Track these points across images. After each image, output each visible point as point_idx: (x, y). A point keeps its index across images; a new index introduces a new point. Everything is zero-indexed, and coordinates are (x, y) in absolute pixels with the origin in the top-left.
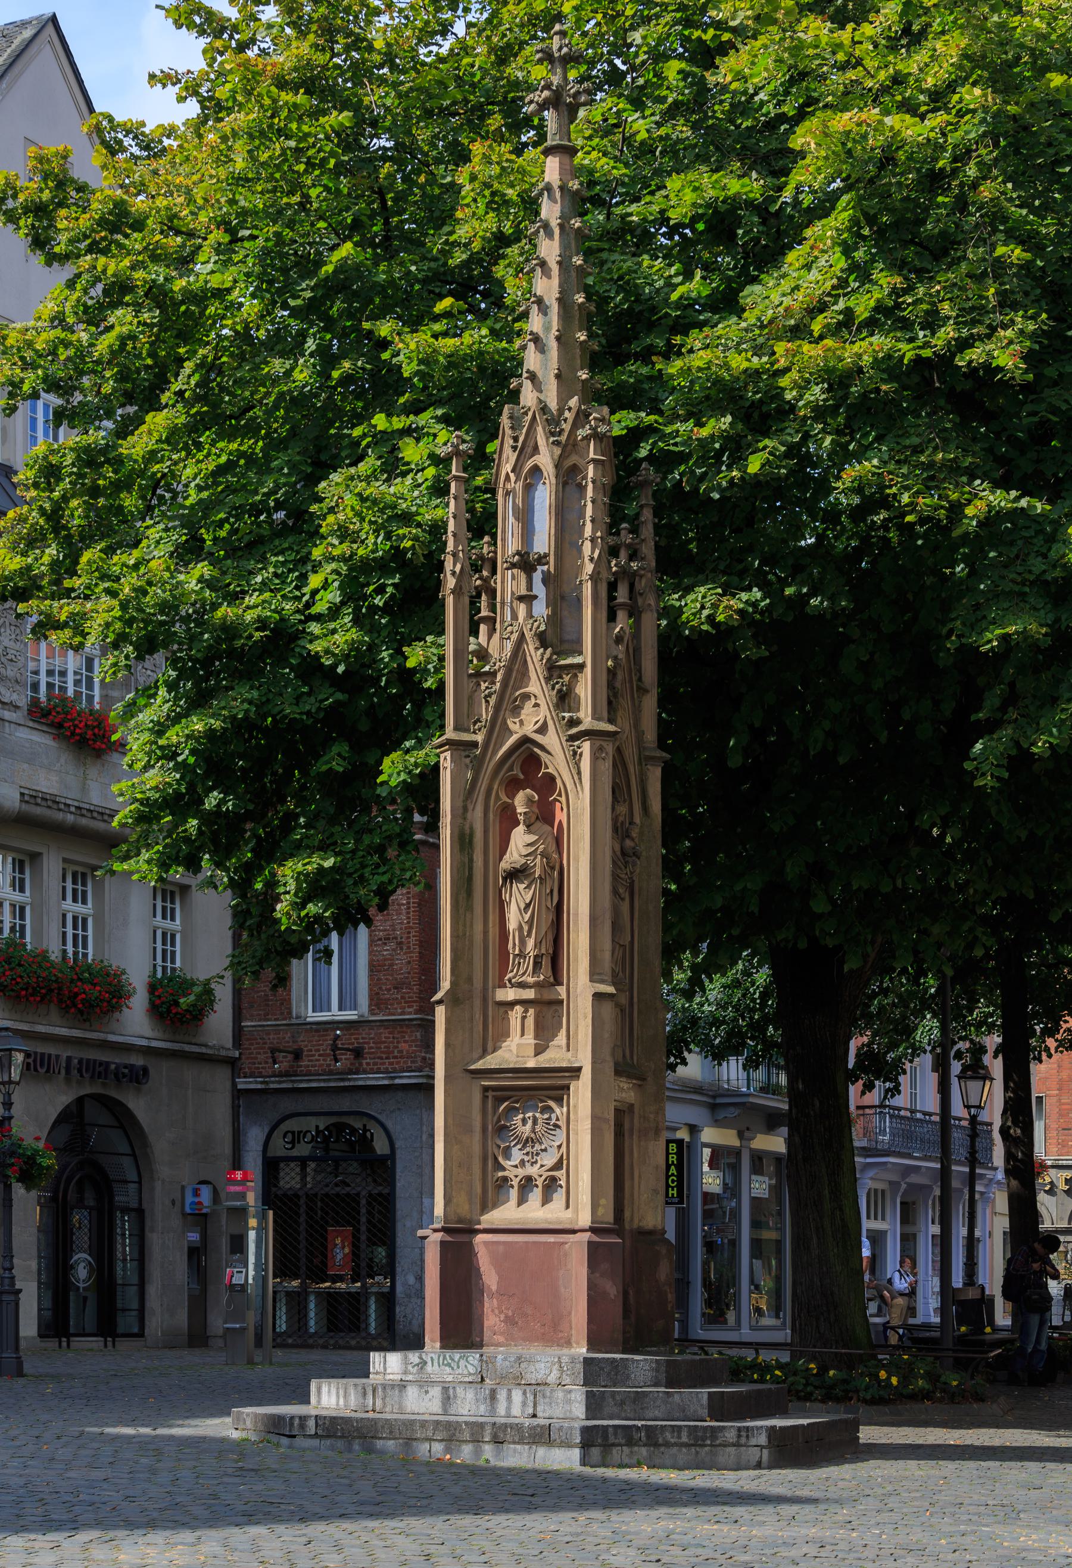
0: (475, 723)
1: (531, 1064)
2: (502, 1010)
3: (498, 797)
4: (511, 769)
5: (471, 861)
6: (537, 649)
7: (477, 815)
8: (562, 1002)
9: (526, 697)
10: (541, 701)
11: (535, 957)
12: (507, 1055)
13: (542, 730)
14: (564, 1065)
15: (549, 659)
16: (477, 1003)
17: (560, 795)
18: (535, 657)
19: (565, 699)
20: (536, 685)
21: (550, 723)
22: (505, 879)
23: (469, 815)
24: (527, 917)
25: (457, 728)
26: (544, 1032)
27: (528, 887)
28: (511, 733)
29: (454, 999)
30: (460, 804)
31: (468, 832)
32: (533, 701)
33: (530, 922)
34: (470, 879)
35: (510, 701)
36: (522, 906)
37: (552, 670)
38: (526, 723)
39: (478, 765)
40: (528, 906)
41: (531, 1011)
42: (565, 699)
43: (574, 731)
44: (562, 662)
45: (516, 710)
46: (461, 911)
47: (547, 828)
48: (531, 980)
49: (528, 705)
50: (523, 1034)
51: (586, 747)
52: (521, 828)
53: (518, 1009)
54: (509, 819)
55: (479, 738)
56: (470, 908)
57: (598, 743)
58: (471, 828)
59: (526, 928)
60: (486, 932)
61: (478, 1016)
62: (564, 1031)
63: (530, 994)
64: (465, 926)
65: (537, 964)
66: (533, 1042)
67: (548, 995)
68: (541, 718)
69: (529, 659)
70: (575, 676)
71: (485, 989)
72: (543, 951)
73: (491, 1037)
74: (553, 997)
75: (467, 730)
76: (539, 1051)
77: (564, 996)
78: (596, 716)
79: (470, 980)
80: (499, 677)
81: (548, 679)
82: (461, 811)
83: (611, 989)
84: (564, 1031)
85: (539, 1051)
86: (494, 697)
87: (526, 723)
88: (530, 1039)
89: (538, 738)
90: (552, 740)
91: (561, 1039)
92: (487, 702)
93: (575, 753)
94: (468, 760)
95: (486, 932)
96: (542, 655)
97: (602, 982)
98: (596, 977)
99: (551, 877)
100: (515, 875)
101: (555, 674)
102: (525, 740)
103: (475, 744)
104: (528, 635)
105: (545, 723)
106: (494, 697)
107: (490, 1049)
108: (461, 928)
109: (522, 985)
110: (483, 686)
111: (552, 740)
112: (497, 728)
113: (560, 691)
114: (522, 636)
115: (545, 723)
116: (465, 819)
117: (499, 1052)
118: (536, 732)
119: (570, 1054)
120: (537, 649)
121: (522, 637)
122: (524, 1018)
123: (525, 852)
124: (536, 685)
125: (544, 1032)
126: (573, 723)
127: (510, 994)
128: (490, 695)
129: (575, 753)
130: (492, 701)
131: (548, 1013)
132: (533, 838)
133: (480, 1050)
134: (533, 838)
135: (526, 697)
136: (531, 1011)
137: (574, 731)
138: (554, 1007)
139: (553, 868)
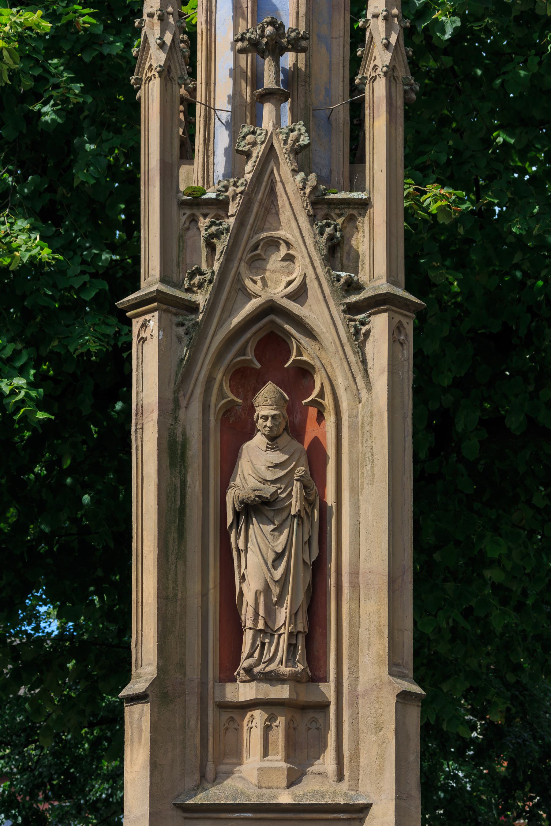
0: (192, 275)
1: (285, 798)
2: (225, 716)
3: (221, 394)
4: (242, 351)
5: (184, 484)
6: (295, 172)
7: (192, 417)
8: (327, 705)
9: (274, 243)
10: (299, 252)
11: (291, 634)
12: (240, 786)
13: (299, 294)
14: (341, 801)
15: (315, 189)
16: (193, 702)
17: (321, 394)
18: (291, 186)
19: (337, 252)
20: (293, 223)
21: (312, 286)
22: (237, 515)
23: (181, 414)
24: (278, 574)
25: (163, 280)
26: (301, 753)
27: (279, 529)
28: (249, 296)
29: (160, 694)
30: (170, 395)
31: (180, 439)
32: (283, 250)
33: (283, 582)
34: (182, 511)
35: (254, 247)
36: (271, 557)
37: (320, 206)
38: (274, 283)
39: (196, 336)
40: (279, 556)
41: (281, 721)
42: (337, 252)
43: (354, 298)
44: (332, 196)
45: (257, 262)
46: (172, 559)
47: (295, 444)
48: (285, 670)
49: (275, 261)
50: (266, 754)
51: (379, 324)
52: (259, 440)
53: (259, 716)
54: (237, 427)
55: (201, 298)
56: (182, 555)
57: (398, 318)
58: (184, 434)
59: (276, 590)
60: (205, 595)
61: (194, 722)
62: (330, 753)
63: (282, 692)
64: (175, 582)
65: (292, 647)
66: (284, 765)
67: (307, 696)
68: (297, 274)
69: (279, 186)
70: (352, 219)
71: (203, 684)
72: (300, 628)
73: (217, 754)
74: (314, 698)
75: (178, 286)
76: (294, 780)
77: (332, 698)
78: (391, 279)
79: (182, 666)
80: (233, 208)
81: (312, 218)
82: (171, 407)
83: (416, 689)
84: (330, 753)
85: (294, 780)
86: (226, 238)
87: (274, 283)
88: (278, 761)
89: (293, 307)
90: (320, 312)
91: (327, 762)
92: (212, 248)
93: (357, 332)
94: (181, 331)
95: (205, 595)
96: (304, 181)
97: (403, 676)
98: (395, 669)
99: (310, 516)
100: (256, 508)
101: (321, 213)
102: (271, 308)
103: (193, 308)
104: (281, 150)
105: (303, 286)
106: (226, 238)
107: (210, 775)
108: (171, 584)
109: (272, 678)
110: (203, 223)
111: (320, 312)
112: (227, 287)
113: (331, 238)
114: (271, 150)
115: (303, 286)
116: (176, 418)
117: (229, 782)
118: (289, 297)
119: (344, 786)
120: (295, 172)
121: (271, 152)
122: (267, 729)
123: (270, 475)
124: (293, 223)
125: (301, 753)
126: (352, 286)
127: (245, 692)
128: (218, 235)
129: (357, 332)
130: (221, 245)
131: (306, 722)
132: (279, 457)
133: (197, 776)
134: (279, 457)
135: (274, 243)
136: (281, 721)
137: (354, 298)
138: (311, 714)
139: (311, 504)
